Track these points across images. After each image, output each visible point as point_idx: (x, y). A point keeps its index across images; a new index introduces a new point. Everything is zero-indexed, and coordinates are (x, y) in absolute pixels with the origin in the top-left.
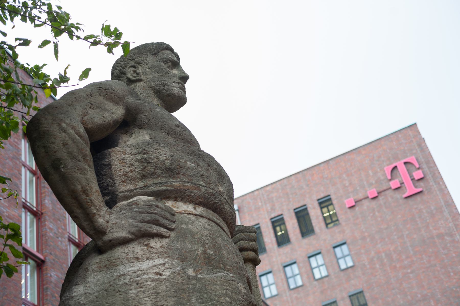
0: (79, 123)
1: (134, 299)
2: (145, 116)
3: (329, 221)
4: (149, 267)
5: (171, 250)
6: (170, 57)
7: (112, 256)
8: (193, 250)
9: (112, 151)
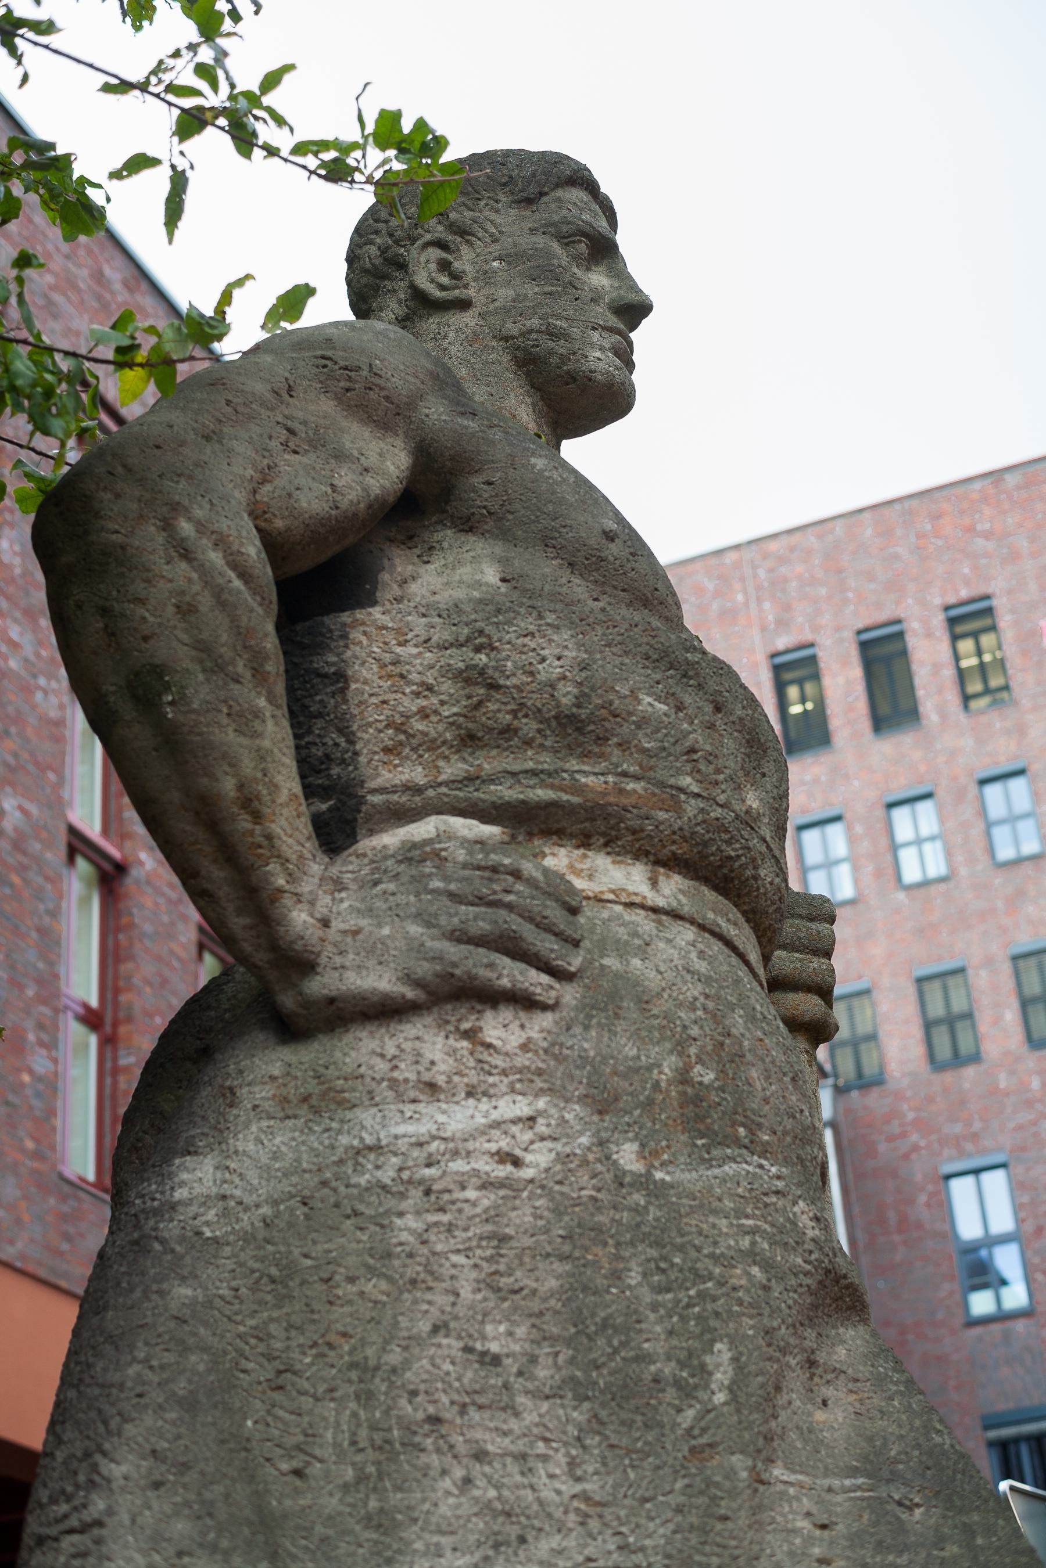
0: (242, 519)
1: (410, 1255)
2: (489, 483)
3: (975, 686)
4: (476, 1129)
5: (560, 1063)
6: (586, 217)
7: (335, 1063)
8: (640, 1068)
9: (353, 626)
